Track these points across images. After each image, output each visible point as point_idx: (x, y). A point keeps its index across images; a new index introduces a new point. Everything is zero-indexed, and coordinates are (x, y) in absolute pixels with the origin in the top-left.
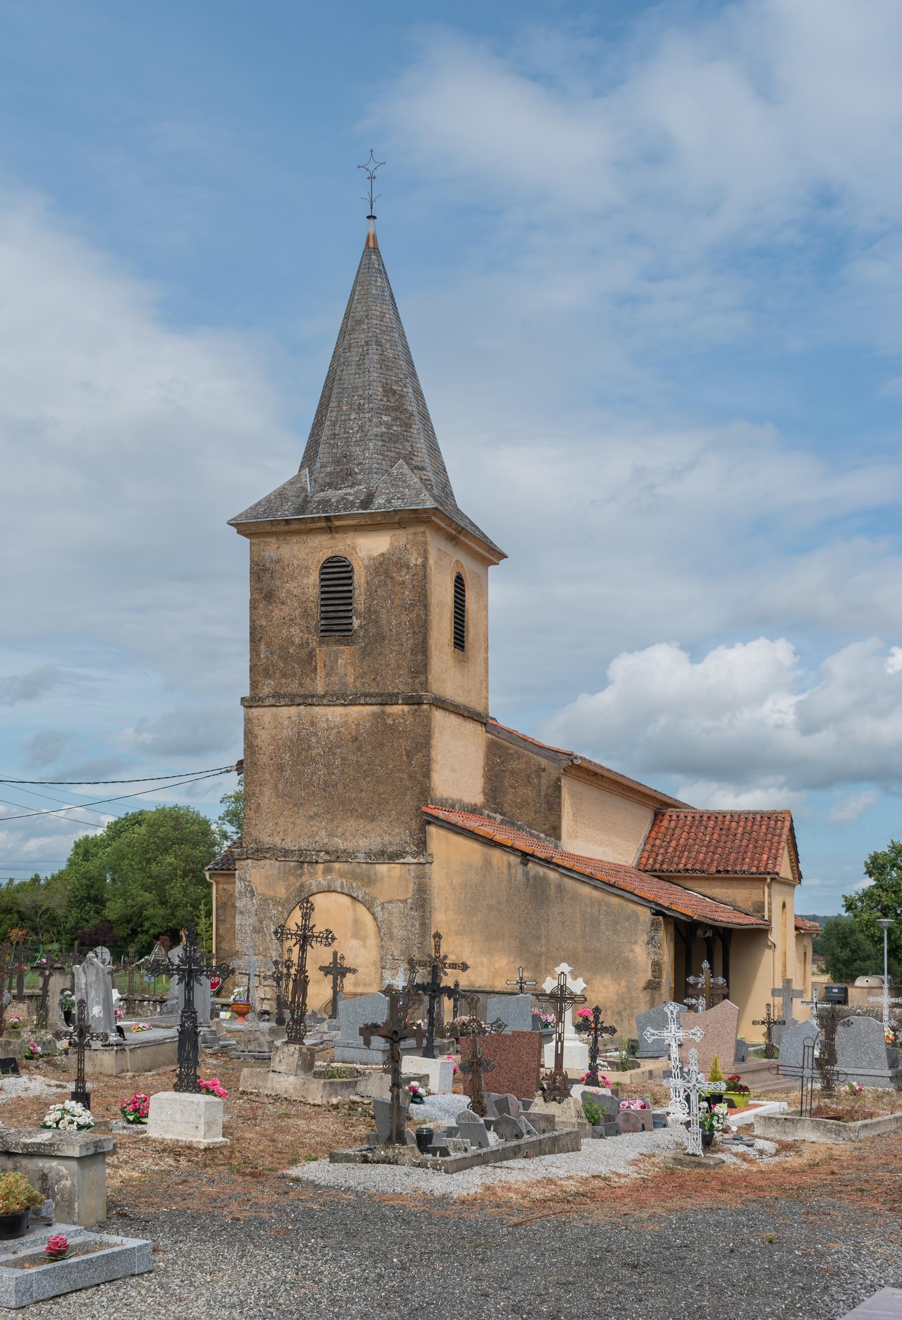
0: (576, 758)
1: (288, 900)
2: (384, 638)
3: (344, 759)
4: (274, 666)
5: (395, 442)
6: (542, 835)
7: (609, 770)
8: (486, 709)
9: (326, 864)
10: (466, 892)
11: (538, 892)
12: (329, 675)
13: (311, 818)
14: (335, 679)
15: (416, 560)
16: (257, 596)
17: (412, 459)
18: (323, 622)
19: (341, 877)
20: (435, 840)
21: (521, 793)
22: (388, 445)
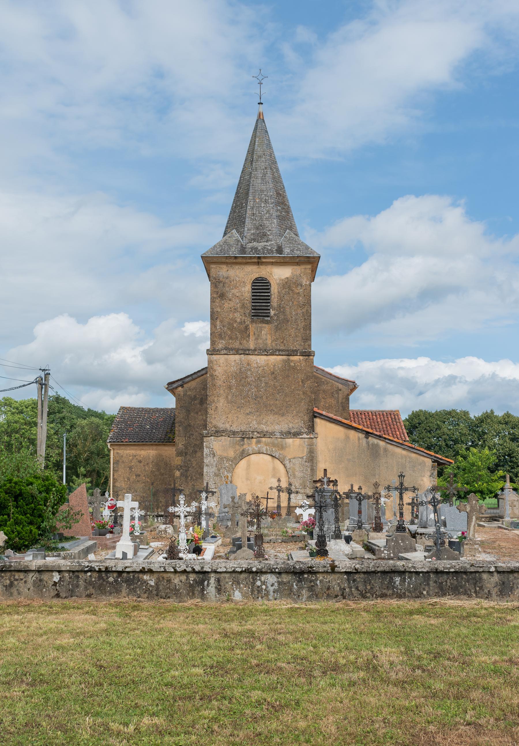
2: (288, 321)
3: (266, 383)
9: (258, 439)
12: (257, 339)
14: (260, 341)
15: (306, 282)
16: (215, 296)
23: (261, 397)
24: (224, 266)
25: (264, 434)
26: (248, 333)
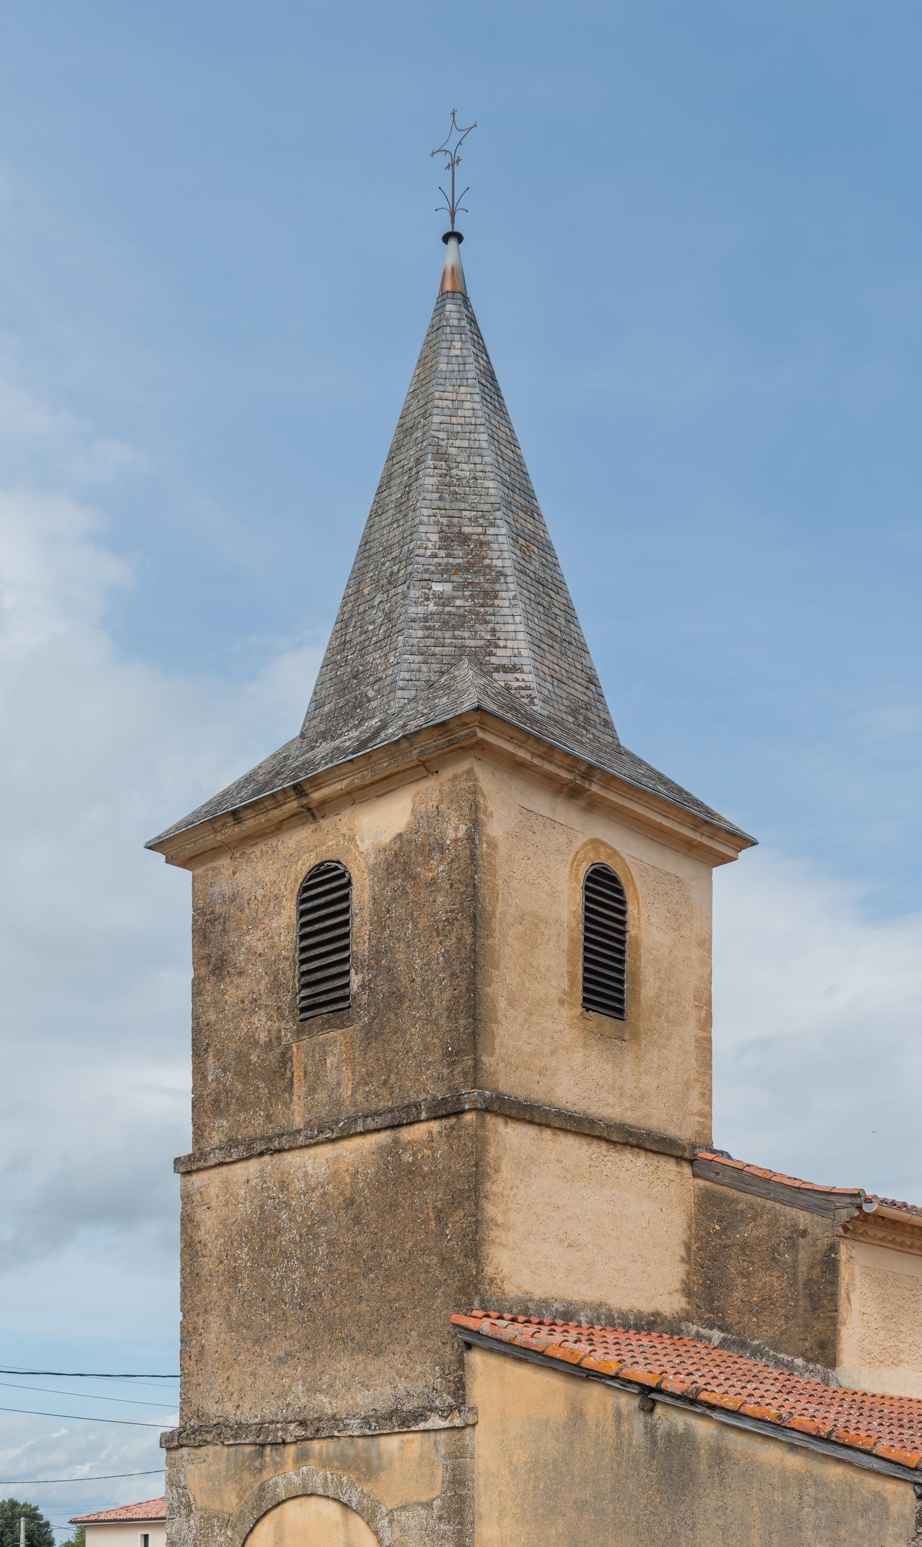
0: (869, 1201)
1: (241, 1515)
2: (401, 999)
3: (331, 1243)
4: (227, 1091)
5: (454, 628)
6: (799, 1361)
7: (822, 1187)
8: (705, 1131)
9: (300, 1445)
10: (537, 1478)
11: (673, 1464)
12: (312, 1090)
13: (281, 1361)
14: (321, 1096)
15: (456, 829)
16: (203, 971)
17: (490, 654)
18: (304, 993)
19: (324, 1466)
20: (480, 1379)
21: (759, 1285)
22: (438, 633)
23: (318, 1297)
24: (224, 863)
25: (313, 1427)
26: (288, 1074)
